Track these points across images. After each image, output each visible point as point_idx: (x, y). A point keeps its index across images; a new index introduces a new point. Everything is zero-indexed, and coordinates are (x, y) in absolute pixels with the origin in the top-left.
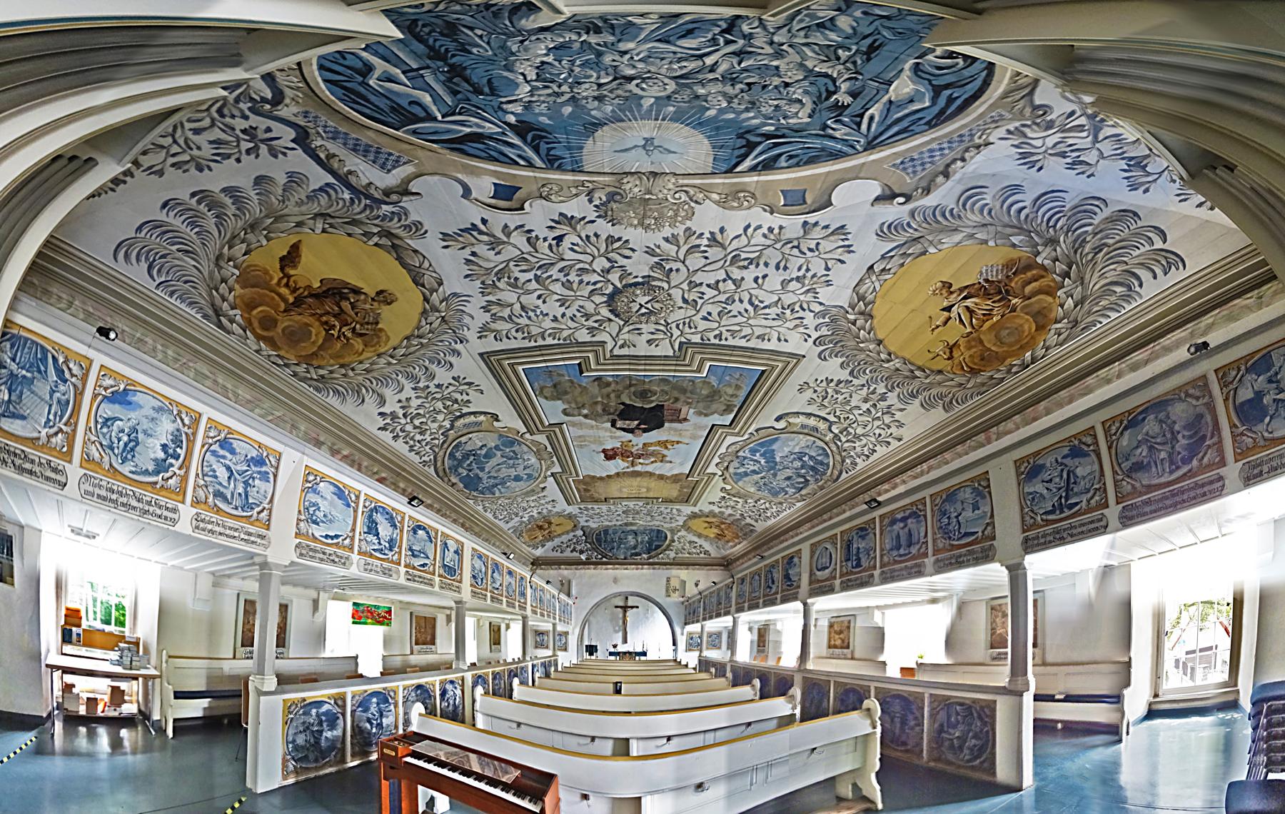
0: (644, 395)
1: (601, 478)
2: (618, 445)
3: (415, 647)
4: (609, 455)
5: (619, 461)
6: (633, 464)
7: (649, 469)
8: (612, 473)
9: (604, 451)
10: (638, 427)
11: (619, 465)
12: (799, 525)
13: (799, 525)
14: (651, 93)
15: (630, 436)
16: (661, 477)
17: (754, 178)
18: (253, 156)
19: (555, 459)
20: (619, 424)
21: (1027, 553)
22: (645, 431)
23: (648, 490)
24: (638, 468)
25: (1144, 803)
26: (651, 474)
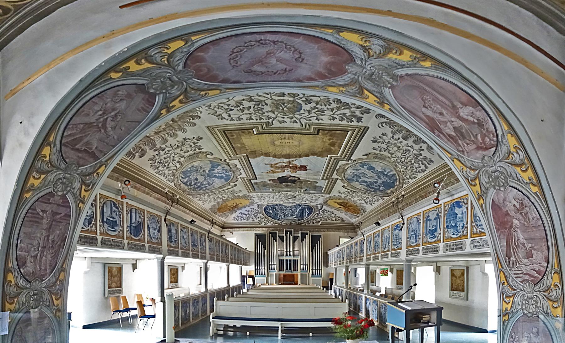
0: (287, 186)
1: (314, 154)
2: (298, 172)
3: (171, 285)
4: (304, 168)
5: (299, 165)
6: (290, 162)
7: (278, 160)
8: (304, 158)
9: (306, 170)
10: (289, 178)
11: (298, 162)
12: (154, 189)
13: (154, 189)
14: (289, 208)
15: (292, 175)
16: (267, 155)
17: (280, 54)
18: (422, 148)
19: (338, 167)
20: (297, 179)
21: (169, 255)
22: (285, 176)
23: (273, 143)
24: (286, 160)
25: (162, 303)
26: (275, 156)
